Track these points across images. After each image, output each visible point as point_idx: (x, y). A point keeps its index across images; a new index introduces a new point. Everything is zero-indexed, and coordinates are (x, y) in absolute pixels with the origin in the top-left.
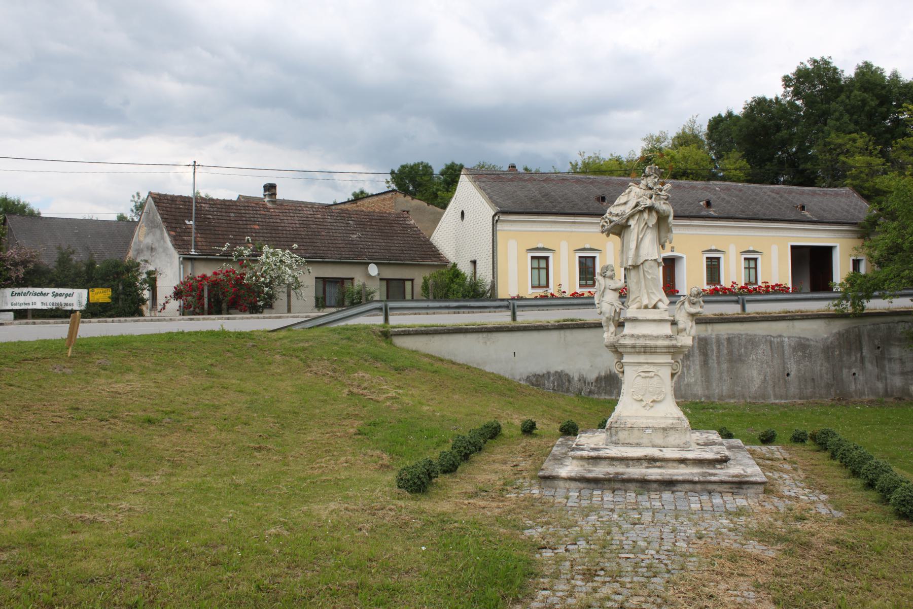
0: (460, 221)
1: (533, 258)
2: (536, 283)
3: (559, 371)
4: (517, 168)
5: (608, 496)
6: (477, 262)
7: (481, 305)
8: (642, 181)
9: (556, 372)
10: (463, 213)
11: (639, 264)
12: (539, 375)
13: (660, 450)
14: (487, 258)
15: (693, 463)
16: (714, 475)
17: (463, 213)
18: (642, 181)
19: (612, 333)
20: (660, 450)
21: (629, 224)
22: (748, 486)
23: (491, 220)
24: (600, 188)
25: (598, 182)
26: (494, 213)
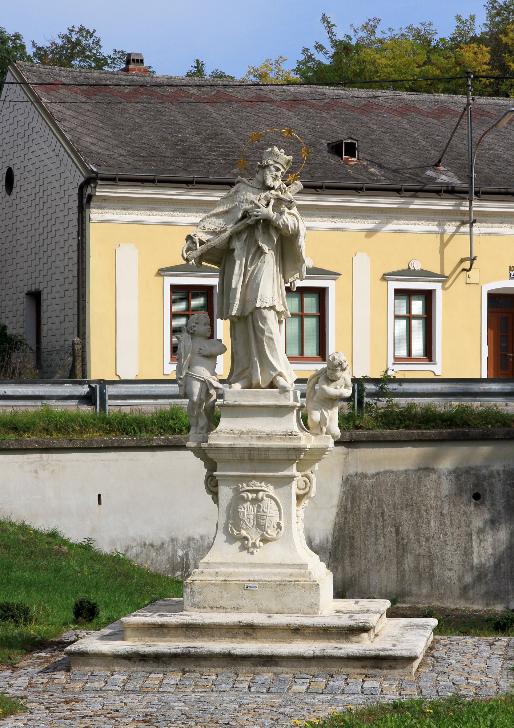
0: (4, 193)
1: (176, 289)
2: (295, 352)
3: (197, 537)
4: (146, 64)
5: (175, 678)
6: (44, 296)
7: (30, 393)
8: (257, 175)
9: (190, 539)
10: (10, 175)
11: (247, 313)
12: (152, 545)
13: (269, 617)
14: (66, 287)
15: (313, 633)
16: (340, 649)
17: (10, 175)
18: (257, 175)
19: (202, 428)
20: (269, 617)
21: (231, 248)
22: (390, 663)
23: (75, 197)
24: (346, 121)
25: (345, 106)
26: (82, 180)
